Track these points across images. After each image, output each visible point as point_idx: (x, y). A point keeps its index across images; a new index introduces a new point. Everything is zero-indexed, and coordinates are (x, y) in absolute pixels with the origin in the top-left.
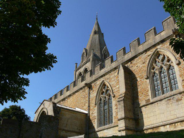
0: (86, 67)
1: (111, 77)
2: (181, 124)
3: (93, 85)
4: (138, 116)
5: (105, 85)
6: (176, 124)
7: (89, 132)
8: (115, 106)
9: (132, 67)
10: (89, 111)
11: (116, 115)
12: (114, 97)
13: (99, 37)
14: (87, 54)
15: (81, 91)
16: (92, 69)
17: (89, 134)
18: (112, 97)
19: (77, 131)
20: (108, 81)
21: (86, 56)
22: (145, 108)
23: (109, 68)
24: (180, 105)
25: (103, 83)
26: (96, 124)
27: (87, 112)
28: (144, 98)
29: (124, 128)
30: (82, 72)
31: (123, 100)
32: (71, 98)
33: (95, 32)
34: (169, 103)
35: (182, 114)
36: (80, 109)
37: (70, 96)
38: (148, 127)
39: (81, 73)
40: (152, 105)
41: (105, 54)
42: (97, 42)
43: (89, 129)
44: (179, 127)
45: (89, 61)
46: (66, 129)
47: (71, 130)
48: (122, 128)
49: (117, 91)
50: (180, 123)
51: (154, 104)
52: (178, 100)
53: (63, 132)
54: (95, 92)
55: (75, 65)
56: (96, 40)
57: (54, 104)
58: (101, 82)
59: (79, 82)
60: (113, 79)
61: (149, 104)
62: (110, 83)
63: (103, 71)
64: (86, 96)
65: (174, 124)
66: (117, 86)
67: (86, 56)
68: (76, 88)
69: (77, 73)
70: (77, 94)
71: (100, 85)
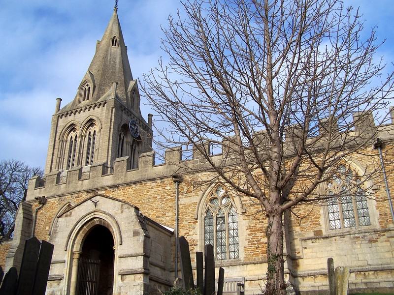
2: (374, 274)
6: (367, 273)
8: (247, 229)
11: (248, 245)
13: (121, 50)
16: (107, 162)
22: (312, 242)
24: (374, 249)
28: (311, 226)
34: (357, 243)
35: (377, 261)
40: (325, 240)
42: (118, 66)
44: (383, 280)
50: (373, 272)
51: (330, 239)
52: (371, 241)
55: (56, 103)
56: (115, 59)
57: (26, 220)
61: (51, 240)
63: (133, 175)
65: (363, 273)
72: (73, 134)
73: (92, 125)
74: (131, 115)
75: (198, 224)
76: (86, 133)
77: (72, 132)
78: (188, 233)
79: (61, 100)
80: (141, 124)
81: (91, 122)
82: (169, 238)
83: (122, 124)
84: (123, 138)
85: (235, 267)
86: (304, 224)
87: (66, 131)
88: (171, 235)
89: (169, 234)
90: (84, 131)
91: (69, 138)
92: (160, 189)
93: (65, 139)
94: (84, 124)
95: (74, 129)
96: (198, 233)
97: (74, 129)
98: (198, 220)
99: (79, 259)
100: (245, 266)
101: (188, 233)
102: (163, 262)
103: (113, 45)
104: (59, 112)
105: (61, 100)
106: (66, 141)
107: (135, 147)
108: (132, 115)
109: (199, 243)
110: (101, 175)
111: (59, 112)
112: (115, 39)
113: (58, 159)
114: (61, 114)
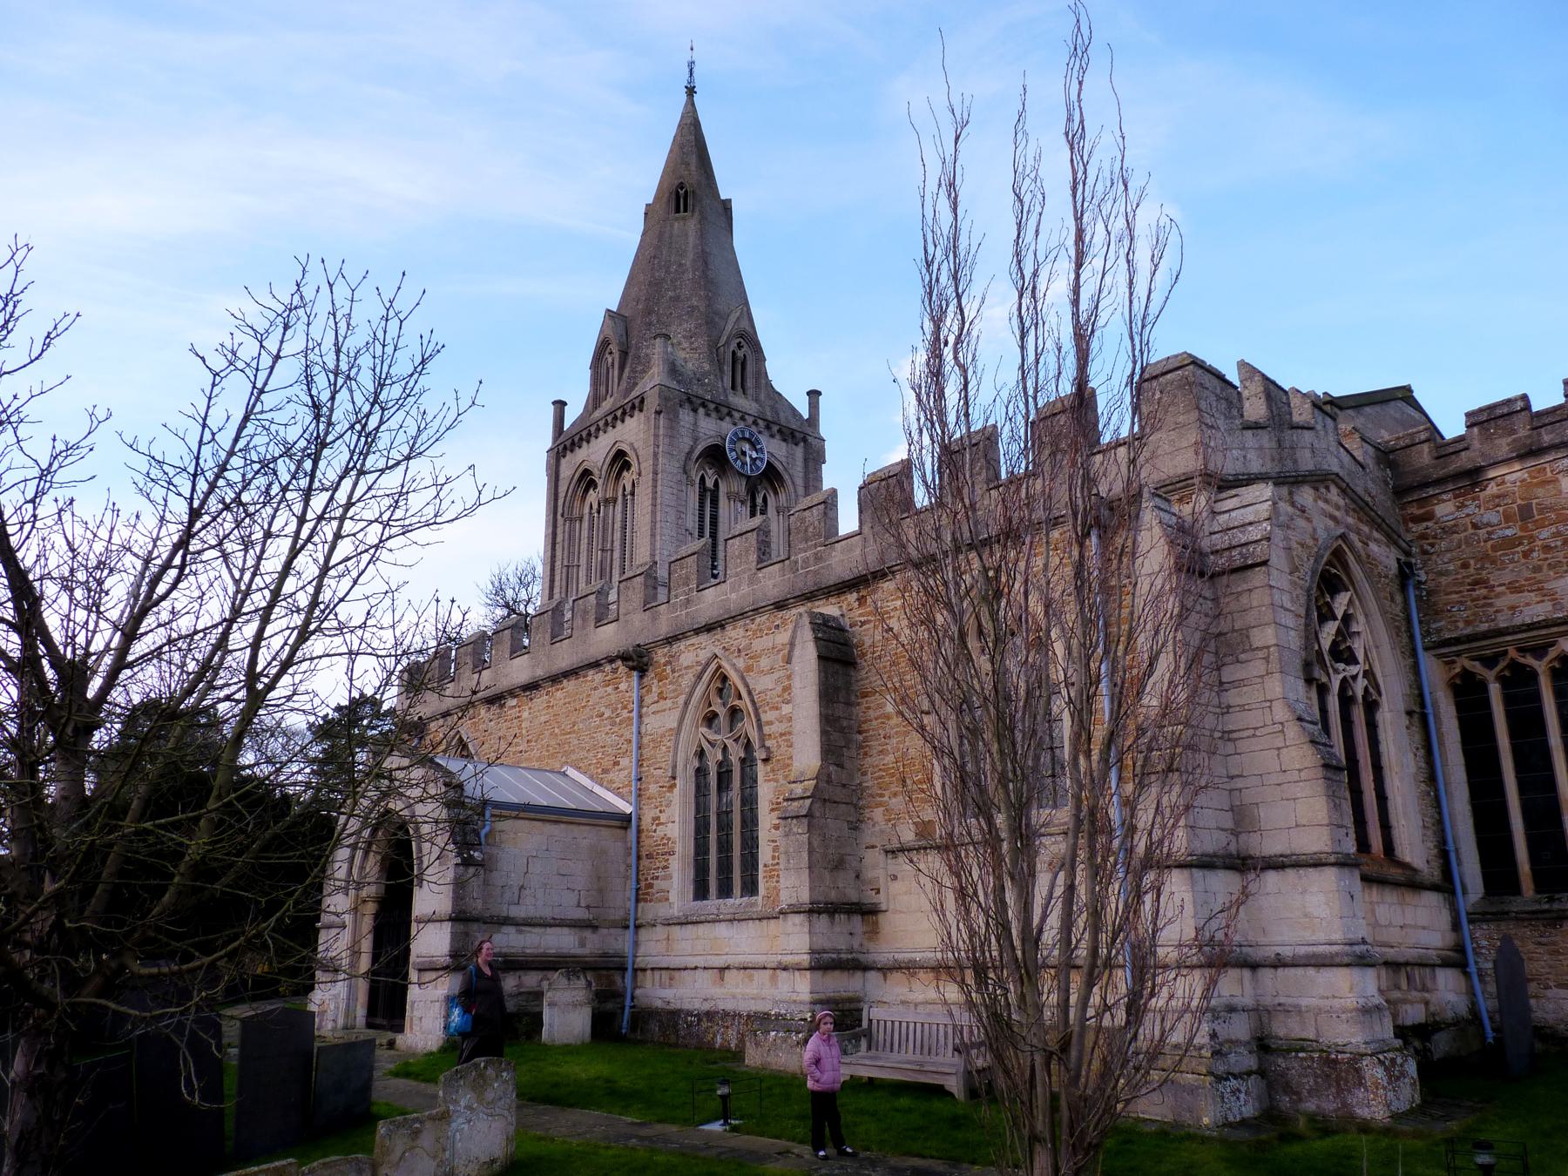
0: (625, 448)
1: (758, 644)
3: (660, 655)
4: (878, 892)
5: (724, 678)
7: (636, 919)
8: (772, 810)
9: (863, 623)
10: (639, 808)
12: (766, 760)
14: (624, 354)
15: (594, 677)
17: (637, 927)
18: (759, 762)
19: (581, 914)
20: (741, 663)
21: (622, 368)
23: (745, 589)
25: (713, 666)
26: (676, 876)
27: (628, 809)
29: (805, 959)
30: (596, 472)
31: (805, 816)
32: (540, 700)
33: (677, 194)
36: (591, 778)
37: (532, 687)
38: (918, 956)
39: (587, 472)
41: (740, 354)
43: (637, 901)
45: (641, 410)
46: (517, 912)
47: (547, 913)
48: (796, 959)
49: (781, 735)
53: (506, 929)
54: (669, 703)
55: (549, 413)
58: (704, 656)
59: (584, 620)
60: (764, 663)
62: (749, 680)
64: (625, 714)
66: (786, 709)
67: (622, 368)
68: (564, 656)
69: (568, 468)
70: (569, 685)
71: (700, 677)
72: (593, 496)
73: (627, 466)
74: (729, 414)
75: (676, 791)
76: (615, 490)
77: (591, 491)
78: (658, 818)
79: (564, 404)
80: (775, 428)
81: (620, 461)
82: (623, 831)
83: (700, 448)
84: (716, 484)
85: (743, 923)
86: (894, 800)
87: (575, 492)
88: (625, 824)
89: (618, 823)
90: (577, 504)
91: (587, 510)
92: (609, 689)
93: (576, 513)
94: (605, 467)
95: (592, 484)
96: (677, 820)
97: (592, 484)
98: (677, 781)
99: (376, 916)
100: (765, 922)
101: (658, 818)
102: (588, 907)
103: (678, 211)
104: (562, 439)
105: (564, 404)
106: (581, 519)
107: (765, 500)
108: (737, 415)
109: (678, 848)
110: (507, 656)
111: (562, 439)
112: (682, 192)
113: (565, 570)
114: (565, 443)
